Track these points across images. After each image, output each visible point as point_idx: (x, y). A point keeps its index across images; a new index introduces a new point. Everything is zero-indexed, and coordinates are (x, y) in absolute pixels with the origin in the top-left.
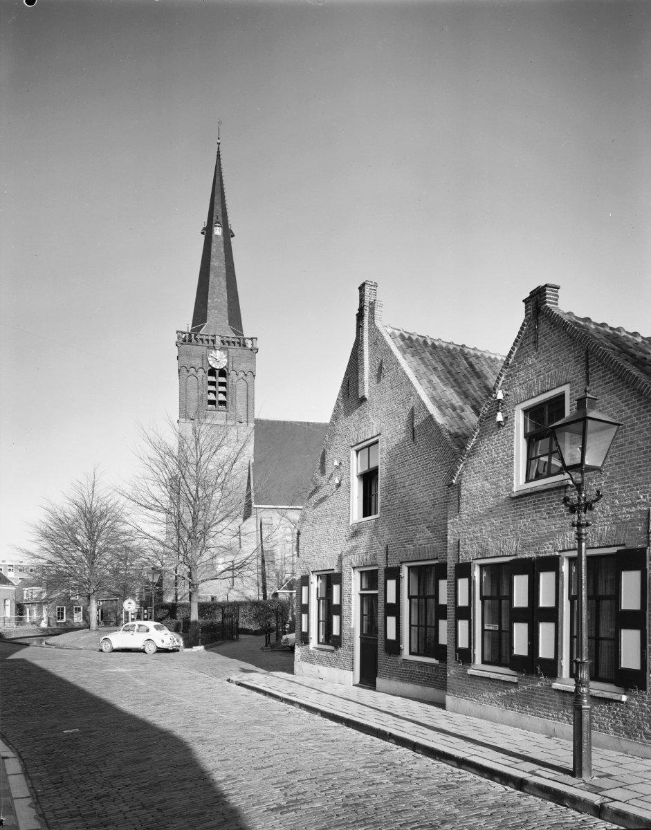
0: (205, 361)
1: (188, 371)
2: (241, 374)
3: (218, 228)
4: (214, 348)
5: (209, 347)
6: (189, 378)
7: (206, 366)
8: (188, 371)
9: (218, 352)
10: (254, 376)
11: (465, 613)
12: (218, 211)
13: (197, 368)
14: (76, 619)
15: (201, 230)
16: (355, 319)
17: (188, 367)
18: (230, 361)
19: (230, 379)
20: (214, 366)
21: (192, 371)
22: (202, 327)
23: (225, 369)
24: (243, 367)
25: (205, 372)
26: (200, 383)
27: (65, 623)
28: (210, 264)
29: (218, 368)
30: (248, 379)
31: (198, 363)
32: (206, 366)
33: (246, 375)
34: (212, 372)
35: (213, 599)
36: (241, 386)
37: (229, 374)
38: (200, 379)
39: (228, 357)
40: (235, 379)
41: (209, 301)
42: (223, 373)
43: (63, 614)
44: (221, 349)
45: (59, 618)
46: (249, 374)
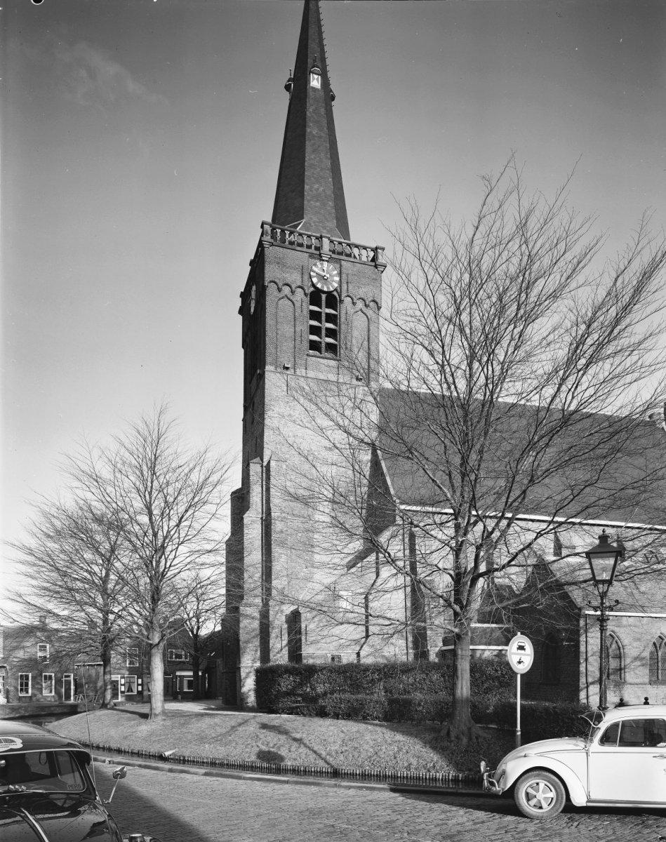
0: (306, 277)
1: (279, 290)
2: (360, 305)
3: (316, 76)
4: (320, 258)
5: (312, 256)
6: (281, 302)
7: (307, 284)
8: (279, 290)
9: (325, 264)
10: (379, 308)
11: (121, 685)
12: (309, 54)
13: (293, 286)
14: (45, 693)
15: (284, 82)
16: (236, 324)
17: (280, 284)
18: (344, 281)
19: (343, 312)
20: (319, 286)
21: (286, 290)
22: (300, 224)
23: (335, 293)
24: (362, 292)
25: (305, 294)
26: (298, 310)
27: (31, 697)
28: (305, 131)
29: (325, 289)
30: (370, 312)
31: (295, 278)
32: (307, 284)
33: (293, 292)
34: (315, 297)
35: (333, 659)
36: (359, 322)
37: (341, 301)
38: (298, 305)
39: (340, 274)
40: (351, 310)
41: (307, 187)
42: (333, 301)
43: (27, 685)
44: (330, 260)
45: (21, 690)
46: (372, 304)
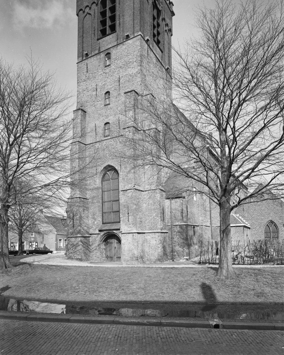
21: (87, 10)
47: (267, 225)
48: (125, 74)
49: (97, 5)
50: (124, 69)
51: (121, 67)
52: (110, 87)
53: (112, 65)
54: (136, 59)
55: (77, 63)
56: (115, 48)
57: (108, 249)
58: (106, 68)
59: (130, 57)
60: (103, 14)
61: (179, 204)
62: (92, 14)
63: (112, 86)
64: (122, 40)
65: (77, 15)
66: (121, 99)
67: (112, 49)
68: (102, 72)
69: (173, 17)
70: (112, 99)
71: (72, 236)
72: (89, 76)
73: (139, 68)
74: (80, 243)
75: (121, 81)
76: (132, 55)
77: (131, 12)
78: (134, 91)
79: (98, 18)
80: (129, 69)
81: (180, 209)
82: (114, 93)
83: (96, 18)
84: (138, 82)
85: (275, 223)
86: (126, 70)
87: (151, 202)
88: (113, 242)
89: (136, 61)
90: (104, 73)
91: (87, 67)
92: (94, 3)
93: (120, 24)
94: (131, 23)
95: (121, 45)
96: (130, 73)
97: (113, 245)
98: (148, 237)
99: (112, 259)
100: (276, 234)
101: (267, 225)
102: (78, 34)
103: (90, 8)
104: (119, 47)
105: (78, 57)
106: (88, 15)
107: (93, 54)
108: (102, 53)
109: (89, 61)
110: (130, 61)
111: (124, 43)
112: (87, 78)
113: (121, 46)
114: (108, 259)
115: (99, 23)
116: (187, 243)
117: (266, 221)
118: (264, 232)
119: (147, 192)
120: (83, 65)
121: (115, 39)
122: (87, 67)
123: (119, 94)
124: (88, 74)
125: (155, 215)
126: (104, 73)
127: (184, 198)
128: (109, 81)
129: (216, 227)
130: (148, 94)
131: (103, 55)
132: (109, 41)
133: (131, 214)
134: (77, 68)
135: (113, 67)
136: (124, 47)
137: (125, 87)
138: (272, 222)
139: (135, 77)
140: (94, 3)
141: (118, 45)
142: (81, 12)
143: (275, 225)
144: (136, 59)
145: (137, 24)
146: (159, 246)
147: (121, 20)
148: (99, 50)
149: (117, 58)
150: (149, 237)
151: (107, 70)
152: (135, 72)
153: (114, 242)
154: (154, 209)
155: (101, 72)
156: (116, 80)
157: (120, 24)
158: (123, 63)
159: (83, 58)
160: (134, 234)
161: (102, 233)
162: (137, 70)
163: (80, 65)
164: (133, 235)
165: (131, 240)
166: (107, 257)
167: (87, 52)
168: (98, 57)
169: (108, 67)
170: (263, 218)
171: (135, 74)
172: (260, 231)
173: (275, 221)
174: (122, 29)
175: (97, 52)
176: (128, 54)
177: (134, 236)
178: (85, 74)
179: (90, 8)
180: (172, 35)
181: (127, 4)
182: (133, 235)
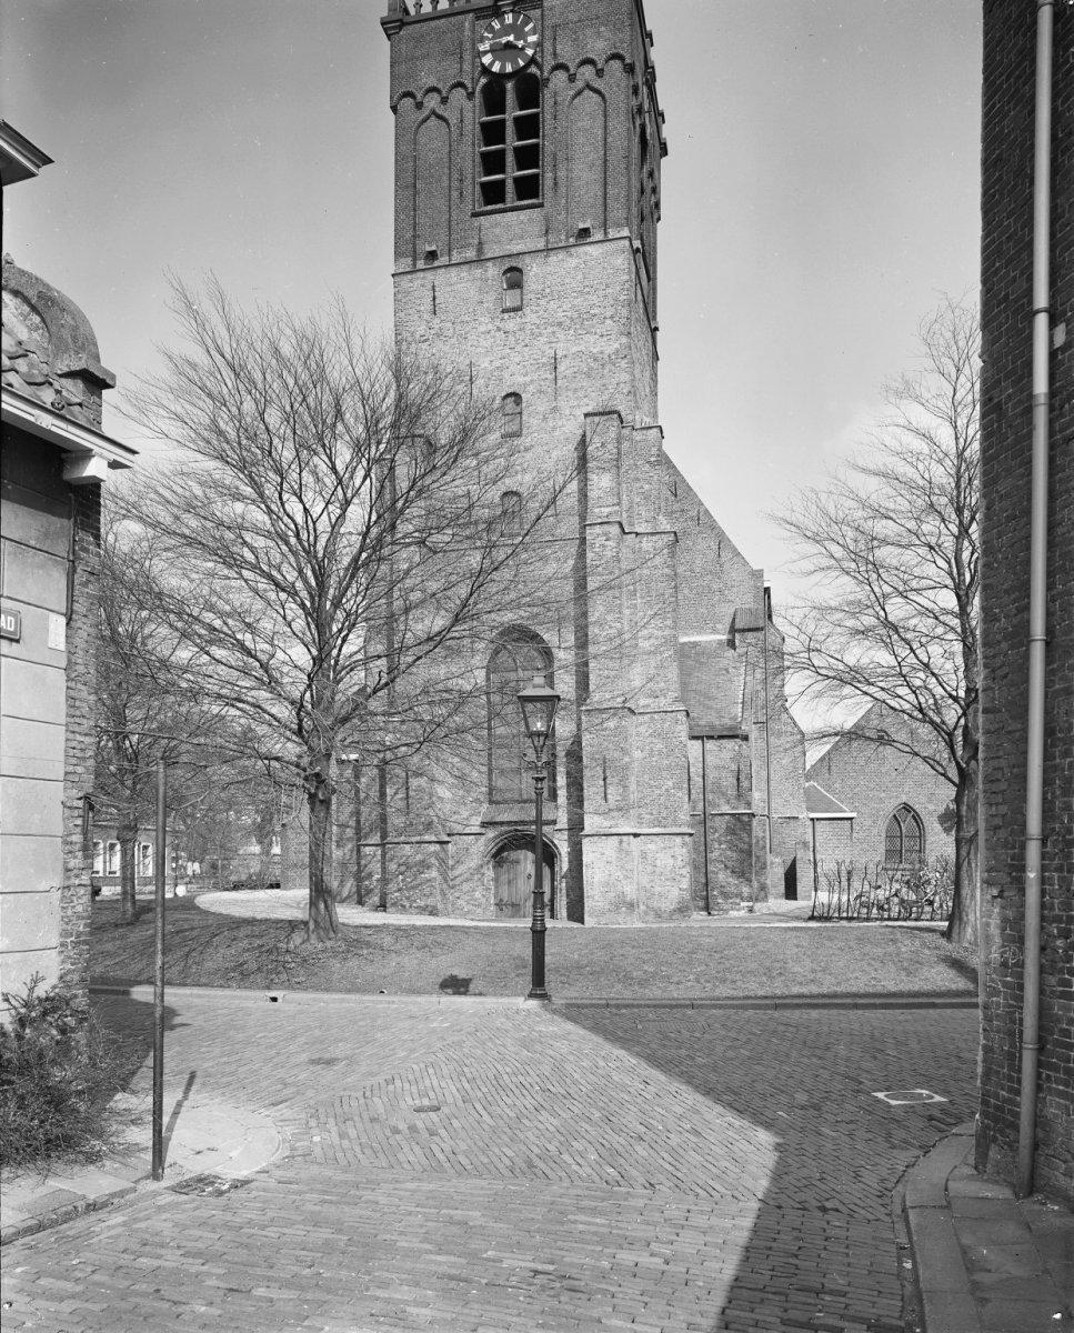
21: (432, 102)
47: (895, 816)
48: (574, 349)
49: (470, 96)
50: (572, 332)
51: (560, 324)
52: (521, 379)
53: (527, 310)
54: (613, 309)
55: (393, 275)
56: (540, 258)
57: (504, 878)
58: (506, 316)
59: (594, 299)
60: (493, 132)
61: (726, 755)
62: (453, 121)
63: (528, 379)
64: (563, 237)
65: (394, 109)
66: (560, 423)
67: (527, 259)
68: (490, 326)
69: (664, 160)
70: (531, 420)
71: (402, 839)
72: (440, 329)
73: (624, 340)
74: (433, 860)
75: (561, 368)
76: (601, 293)
77: (595, 156)
78: (620, 416)
79: (471, 148)
80: (592, 338)
81: (734, 767)
82: (538, 402)
83: (468, 139)
84: (622, 385)
85: (914, 810)
86: (578, 336)
87: (660, 746)
88: (522, 857)
89: (612, 317)
90: (499, 329)
91: (434, 299)
92: (460, 85)
93: (556, 184)
94: (597, 190)
95: (561, 255)
96: (595, 351)
97: (521, 867)
98: (650, 846)
99: (519, 910)
100: (918, 844)
101: (895, 816)
102: (396, 176)
103: (444, 100)
104: (553, 258)
105: (398, 255)
106: (433, 118)
107: (456, 258)
108: (490, 264)
109: (440, 277)
110: (592, 312)
111: (573, 250)
112: (433, 332)
113: (561, 257)
114: (501, 910)
115: (478, 159)
116: (747, 863)
117: (890, 806)
118: (884, 835)
119: (647, 717)
120: (419, 284)
121: (537, 228)
122: (434, 299)
123: (555, 409)
124: (437, 321)
125: (670, 783)
126: (499, 329)
127: (746, 738)
128: (517, 360)
129: (780, 820)
130: (651, 428)
131: (493, 271)
132: (513, 229)
133: (616, 780)
134: (392, 291)
135: (530, 316)
136: (573, 262)
137: (576, 390)
138: (907, 808)
139: (608, 367)
140: (460, 85)
141: (548, 250)
142: (408, 102)
143: (917, 818)
144: (613, 309)
145: (617, 200)
146: (684, 871)
147: (562, 174)
148: (480, 247)
149: (548, 290)
150: (652, 847)
151: (512, 323)
152: (609, 350)
153: (526, 859)
154: (669, 767)
155: (485, 324)
156: (544, 364)
157: (556, 184)
158: (569, 314)
159: (415, 260)
160: (625, 838)
161: (491, 833)
162: (617, 345)
163: (405, 282)
164: (621, 842)
165: (614, 855)
166: (500, 905)
167: (434, 248)
168: (478, 272)
169: (512, 314)
170: (883, 795)
171: (609, 356)
172: (875, 831)
173: (916, 807)
174: (564, 201)
175: (471, 254)
176: (587, 289)
177: (624, 844)
178: (426, 316)
179: (444, 100)
180: (659, 219)
181: (580, 124)
182: (621, 842)
